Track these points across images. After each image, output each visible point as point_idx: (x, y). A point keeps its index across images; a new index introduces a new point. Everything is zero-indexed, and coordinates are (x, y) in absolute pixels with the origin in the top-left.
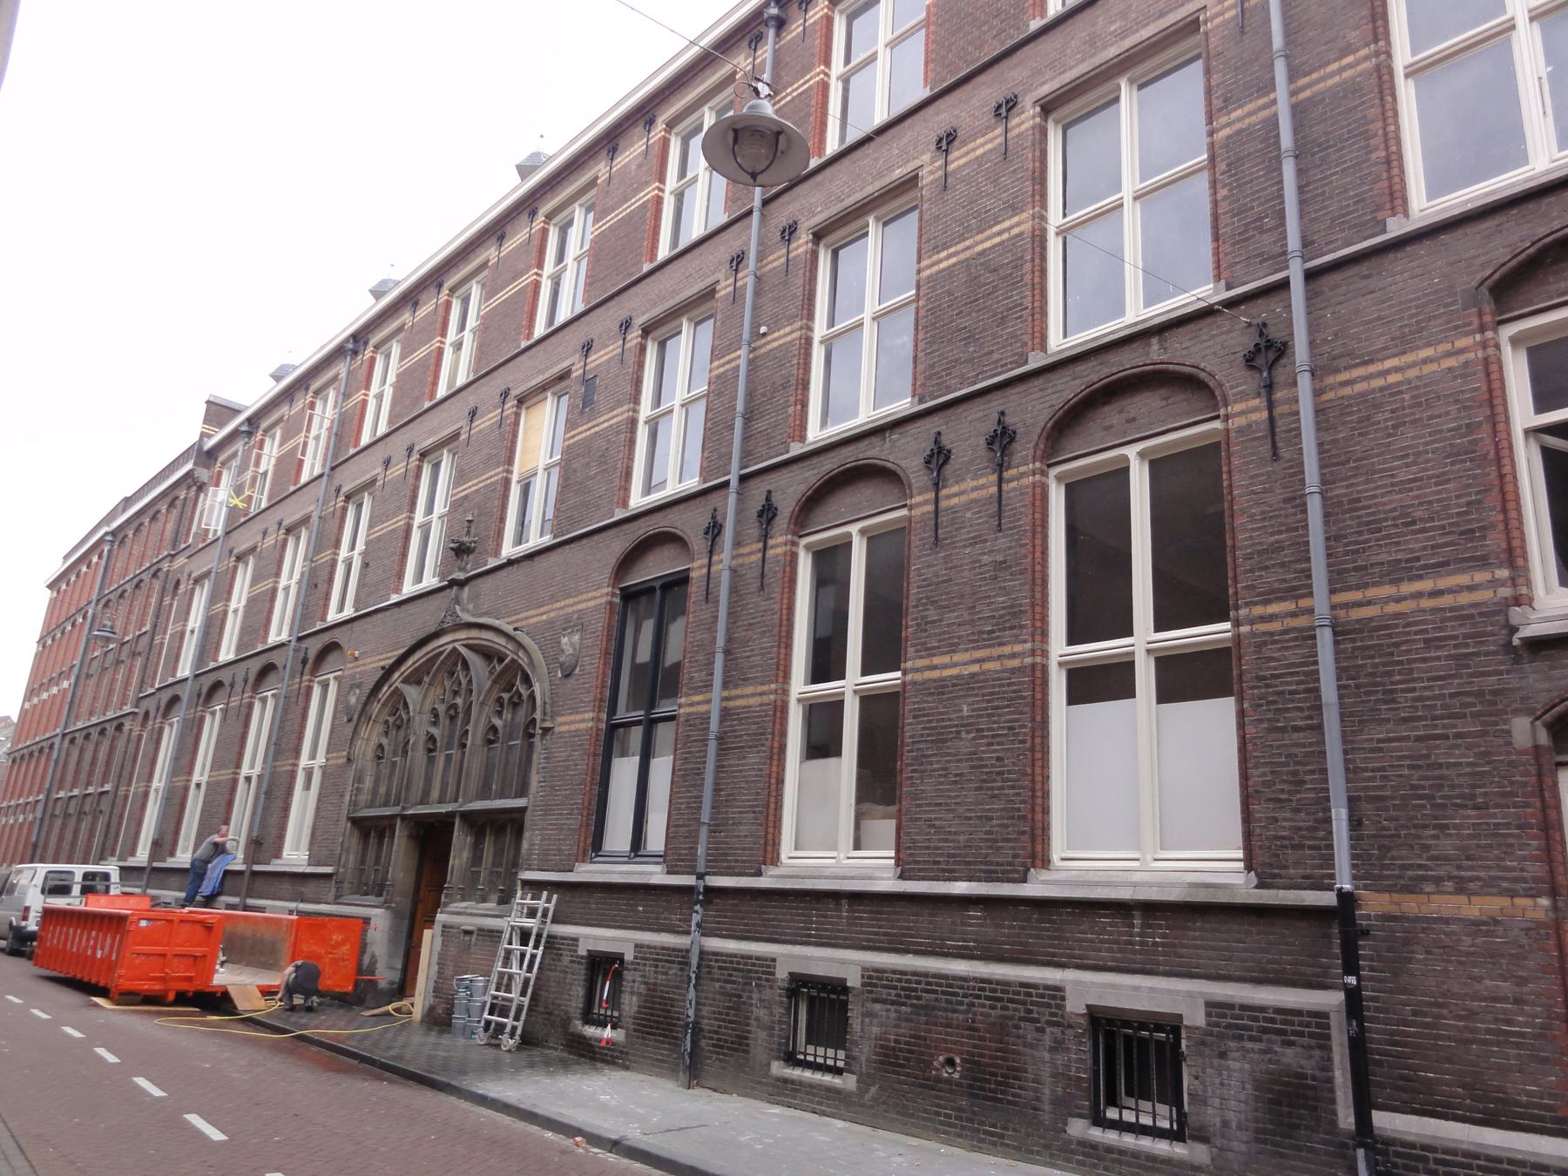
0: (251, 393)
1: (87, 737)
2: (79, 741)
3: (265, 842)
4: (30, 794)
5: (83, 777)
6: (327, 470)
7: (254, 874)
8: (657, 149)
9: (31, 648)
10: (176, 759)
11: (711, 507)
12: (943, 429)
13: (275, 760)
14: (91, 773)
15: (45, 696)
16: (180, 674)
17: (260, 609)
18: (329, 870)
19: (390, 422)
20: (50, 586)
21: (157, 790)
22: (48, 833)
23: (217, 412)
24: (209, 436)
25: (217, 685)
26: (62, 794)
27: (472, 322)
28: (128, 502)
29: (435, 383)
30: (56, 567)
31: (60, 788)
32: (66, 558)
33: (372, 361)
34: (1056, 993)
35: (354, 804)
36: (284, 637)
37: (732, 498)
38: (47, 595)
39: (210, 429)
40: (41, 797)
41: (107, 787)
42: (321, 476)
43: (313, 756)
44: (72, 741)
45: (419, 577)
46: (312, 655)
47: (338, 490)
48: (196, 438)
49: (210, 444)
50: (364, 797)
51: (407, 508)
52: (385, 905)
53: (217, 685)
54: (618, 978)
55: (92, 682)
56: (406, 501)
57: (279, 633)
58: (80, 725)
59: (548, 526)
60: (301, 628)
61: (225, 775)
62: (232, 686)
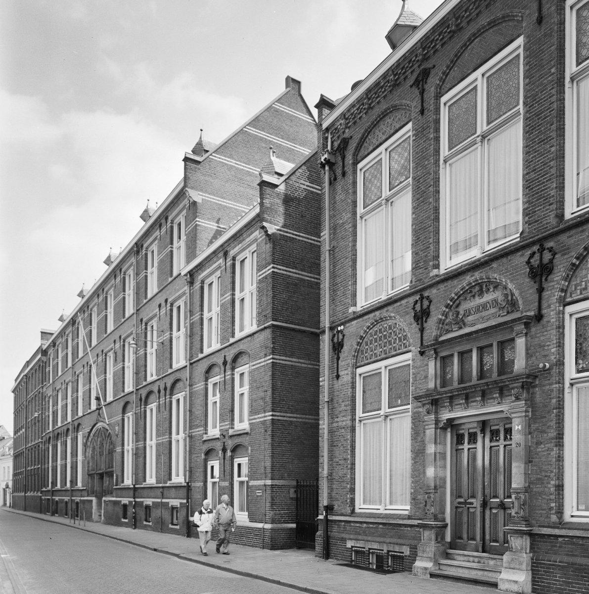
0: (55, 327)
1: (35, 447)
2: (34, 449)
3: (74, 482)
4: (35, 465)
5: (37, 463)
6: (135, 311)
7: (72, 490)
8: (169, 230)
9: (12, 416)
10: (136, 433)
11: (223, 355)
12: (226, 354)
13: (190, 428)
14: (35, 461)
15: (19, 434)
16: (127, 390)
17: (166, 350)
18: (85, 488)
19: (62, 371)
20: (13, 392)
21: (128, 451)
22: (28, 481)
23: (44, 334)
24: (45, 345)
25: (150, 393)
26: (29, 468)
27: (156, 264)
28: (28, 363)
29: (58, 372)
30: (12, 385)
31: (28, 466)
32: (16, 380)
33: (146, 255)
34: (168, 503)
35: (88, 470)
36: (131, 389)
37: (135, 395)
38: (13, 395)
39: (44, 342)
40: (39, 466)
41: (39, 466)
42: (134, 314)
43: (178, 433)
44: (28, 450)
45: (210, 346)
46: (169, 386)
47: (142, 320)
48: (40, 345)
49: (44, 347)
50: (107, 466)
51: (169, 329)
52: (96, 496)
53: (150, 393)
54: (150, 509)
55: (30, 429)
56: (230, 287)
57: (129, 387)
58: (30, 445)
59: (255, 321)
60: (137, 386)
61: (165, 439)
62: (159, 391)
